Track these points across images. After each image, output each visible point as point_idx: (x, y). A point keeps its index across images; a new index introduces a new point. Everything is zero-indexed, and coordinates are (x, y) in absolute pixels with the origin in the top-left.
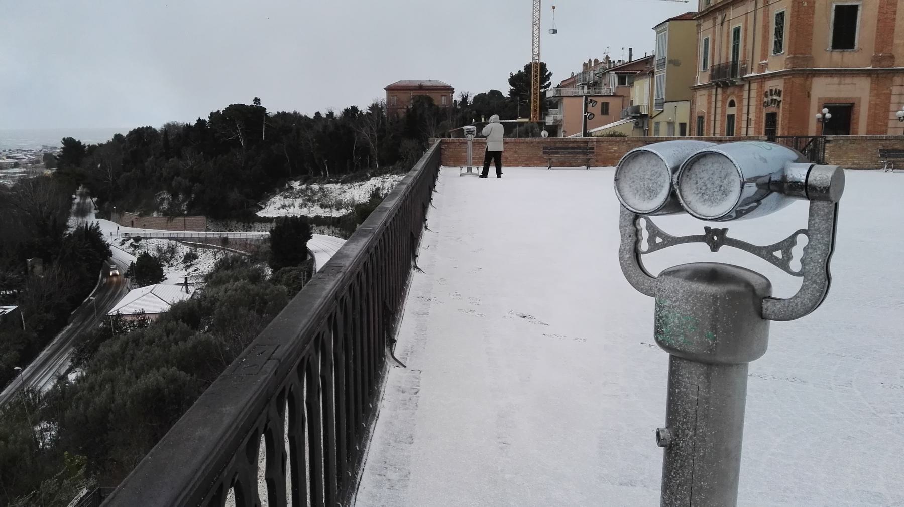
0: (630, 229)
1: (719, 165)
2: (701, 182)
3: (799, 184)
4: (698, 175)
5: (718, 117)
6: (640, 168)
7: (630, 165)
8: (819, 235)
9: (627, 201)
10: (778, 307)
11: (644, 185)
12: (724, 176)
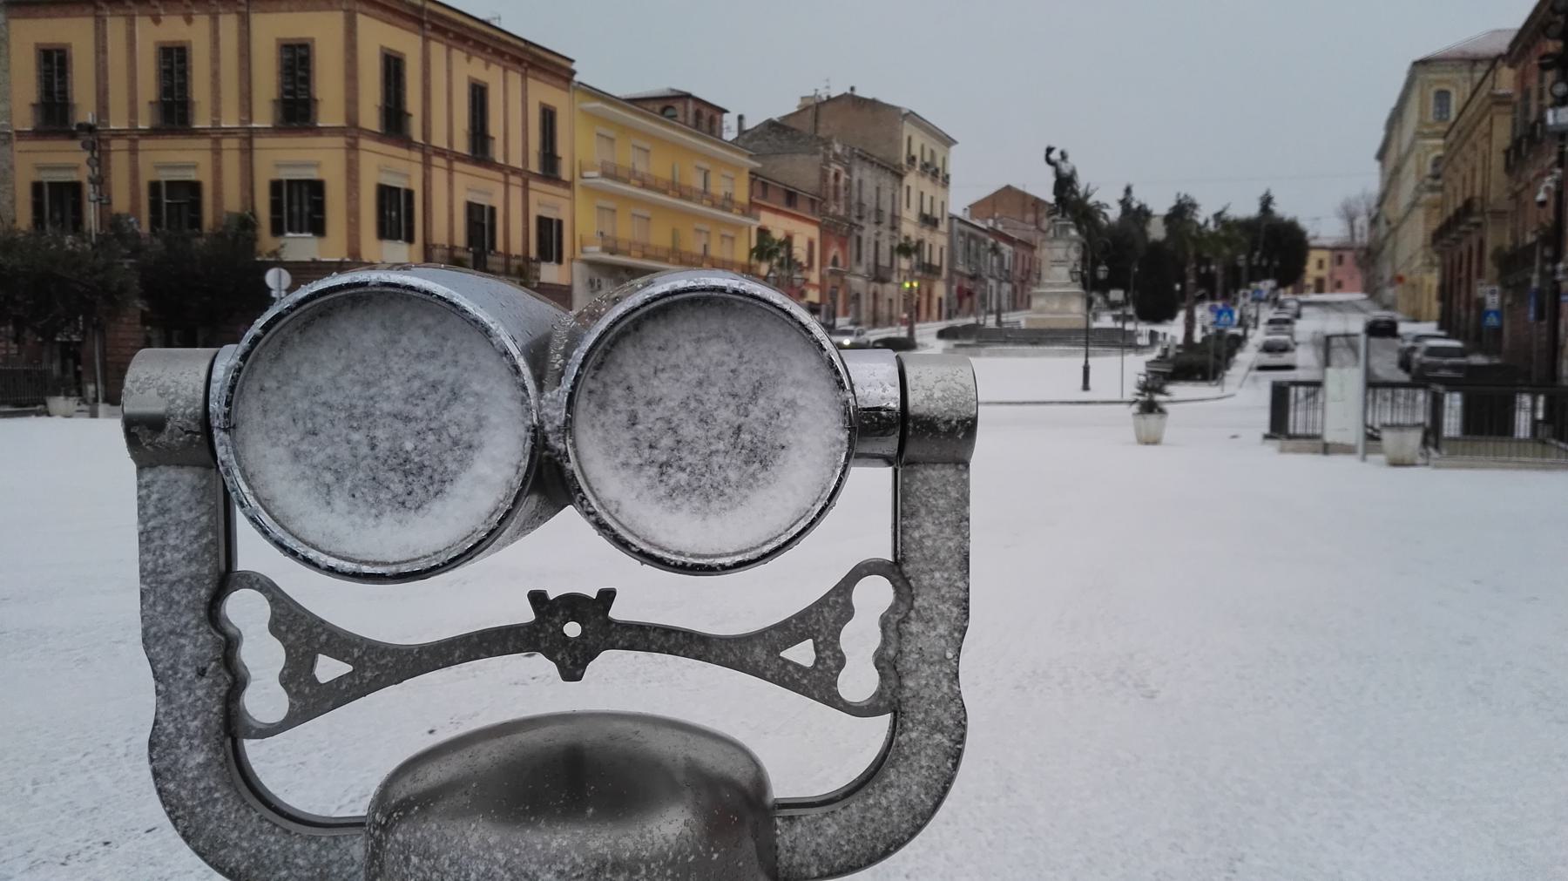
0: (196, 645)
1: (726, 347)
2: (652, 417)
3: (884, 413)
4: (640, 391)
6: (347, 367)
7: (290, 358)
8: (937, 575)
9: (295, 527)
10: (830, 832)
11: (373, 447)
12: (749, 388)
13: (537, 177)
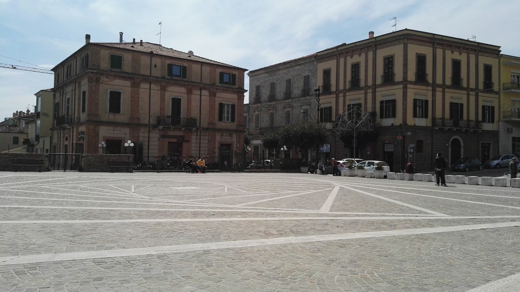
5: (61, 146)
13: (483, 91)
